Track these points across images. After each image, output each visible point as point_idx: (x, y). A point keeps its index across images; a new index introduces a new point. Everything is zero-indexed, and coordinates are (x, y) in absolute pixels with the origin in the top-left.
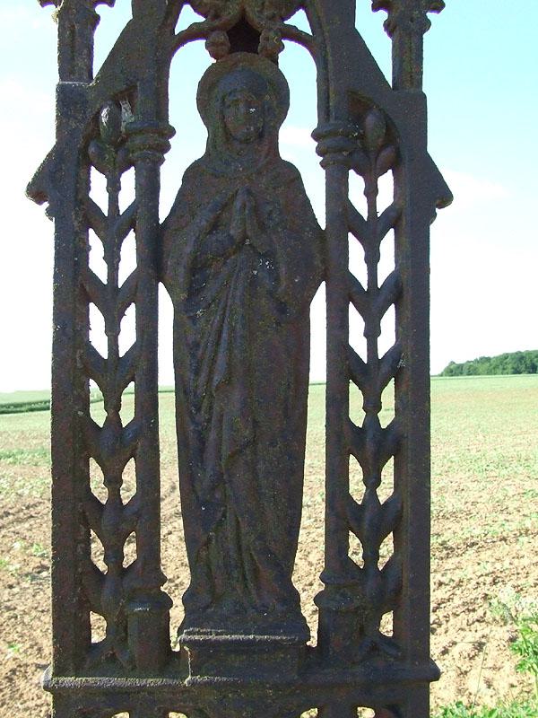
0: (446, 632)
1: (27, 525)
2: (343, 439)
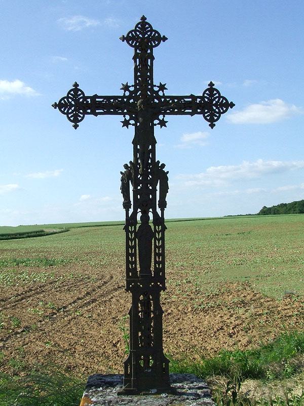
0: (237, 337)
1: (42, 295)
2: (156, 254)
